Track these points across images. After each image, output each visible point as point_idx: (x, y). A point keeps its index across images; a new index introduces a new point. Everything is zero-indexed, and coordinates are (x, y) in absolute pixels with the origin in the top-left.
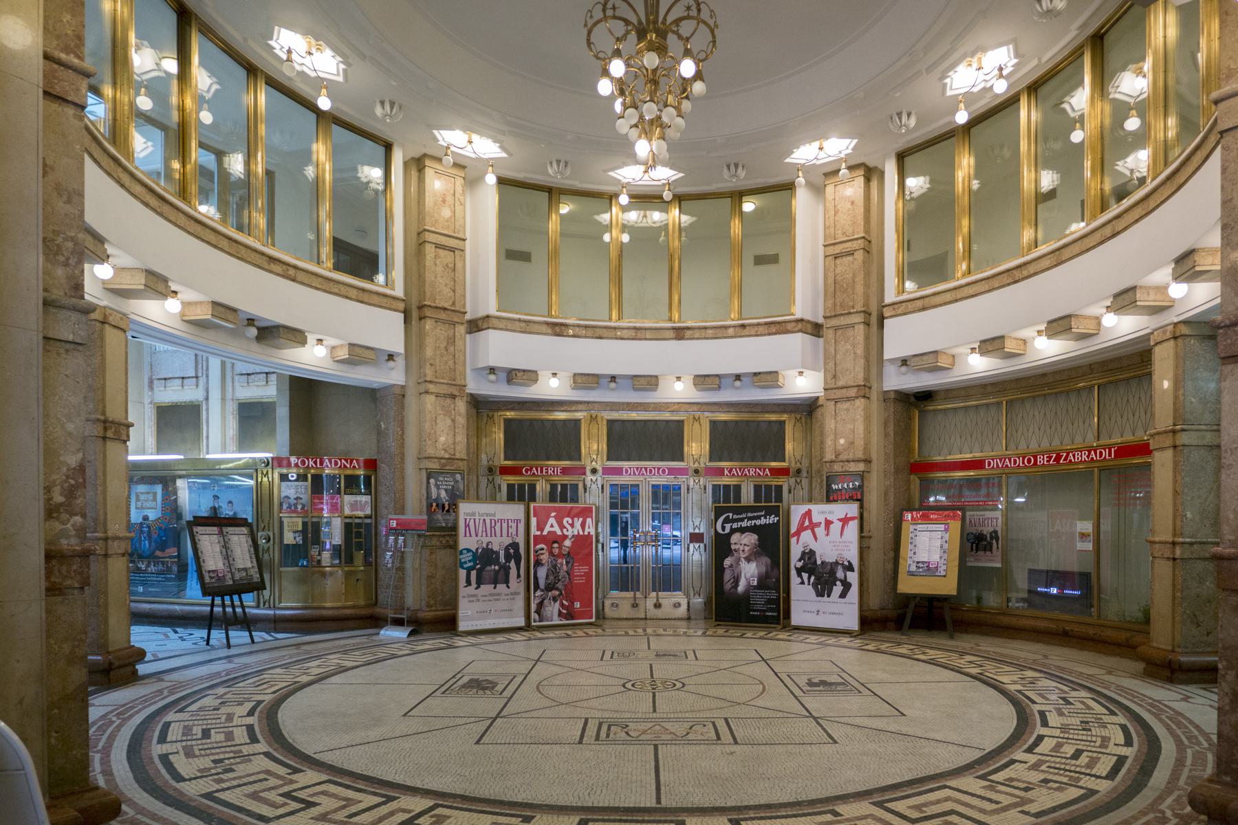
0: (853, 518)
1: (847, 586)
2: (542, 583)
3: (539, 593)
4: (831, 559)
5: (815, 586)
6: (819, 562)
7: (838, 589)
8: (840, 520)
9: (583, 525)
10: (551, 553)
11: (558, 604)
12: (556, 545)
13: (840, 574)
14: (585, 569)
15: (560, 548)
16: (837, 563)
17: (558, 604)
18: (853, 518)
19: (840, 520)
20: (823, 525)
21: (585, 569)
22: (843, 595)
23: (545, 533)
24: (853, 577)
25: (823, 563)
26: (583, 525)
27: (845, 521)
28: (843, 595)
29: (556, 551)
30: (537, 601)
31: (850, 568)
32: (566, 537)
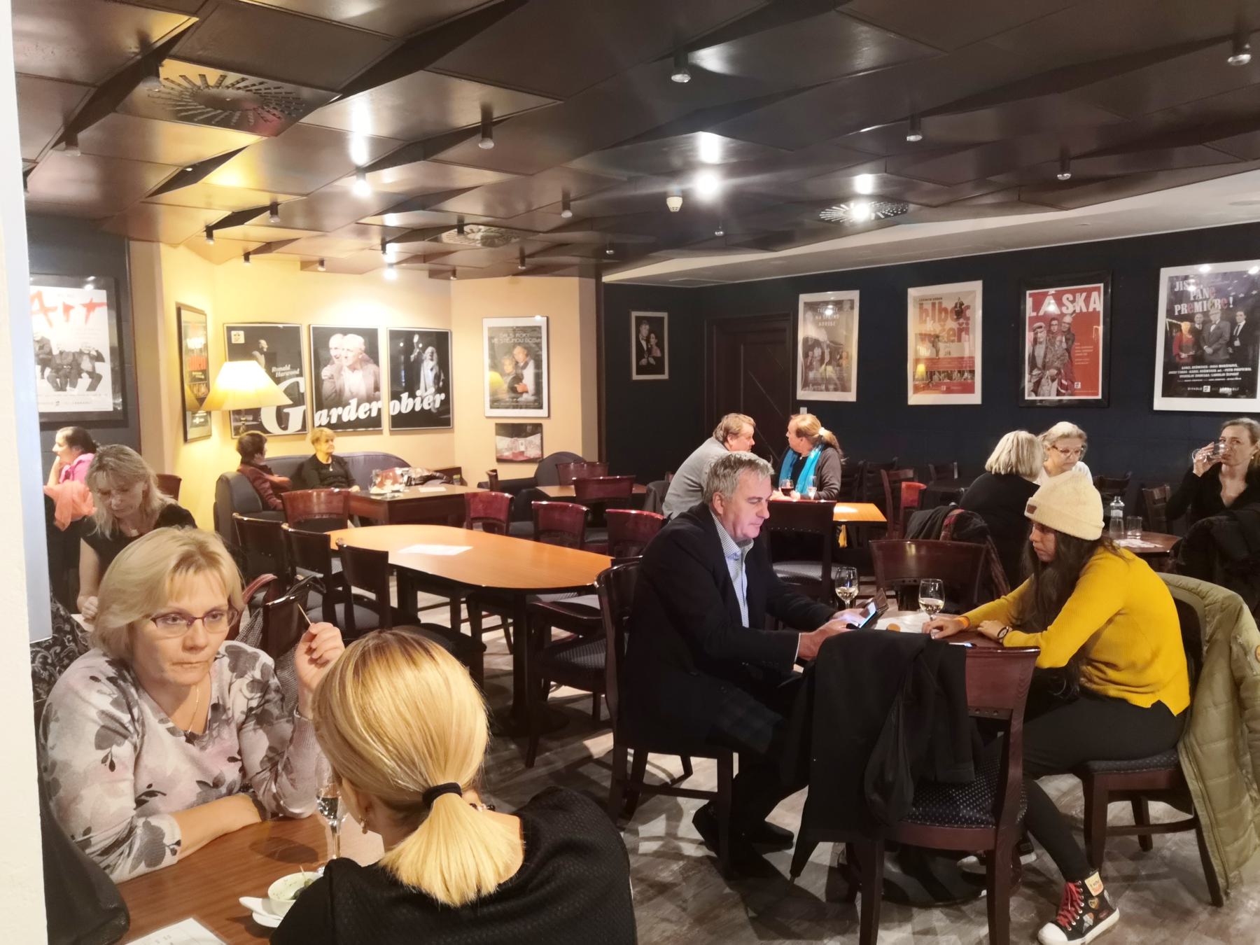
0: (100, 305)
1: (96, 378)
2: (1039, 362)
3: (1035, 372)
4: (72, 347)
5: (52, 381)
6: (55, 352)
7: (85, 380)
8: (84, 305)
9: (1087, 300)
10: (1049, 331)
11: (1056, 383)
12: (1054, 322)
13: (86, 364)
14: (1088, 349)
15: (1060, 324)
16: (81, 353)
17: (1056, 383)
18: (100, 305)
19: (84, 305)
20: (61, 309)
21: (1088, 349)
22: (92, 387)
23: (1041, 313)
24: (105, 369)
25: (61, 353)
26: (1087, 300)
27: (91, 307)
28: (92, 387)
29: (1055, 328)
30: (1034, 380)
31: (99, 358)
32: (1063, 315)
